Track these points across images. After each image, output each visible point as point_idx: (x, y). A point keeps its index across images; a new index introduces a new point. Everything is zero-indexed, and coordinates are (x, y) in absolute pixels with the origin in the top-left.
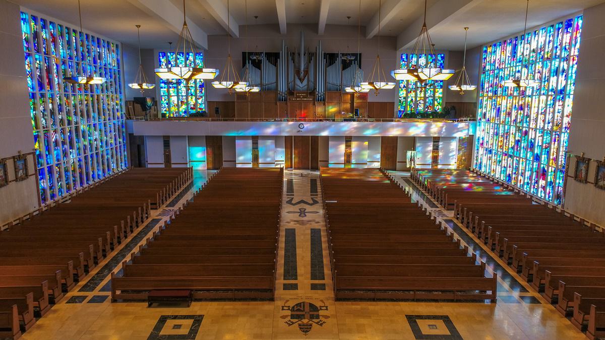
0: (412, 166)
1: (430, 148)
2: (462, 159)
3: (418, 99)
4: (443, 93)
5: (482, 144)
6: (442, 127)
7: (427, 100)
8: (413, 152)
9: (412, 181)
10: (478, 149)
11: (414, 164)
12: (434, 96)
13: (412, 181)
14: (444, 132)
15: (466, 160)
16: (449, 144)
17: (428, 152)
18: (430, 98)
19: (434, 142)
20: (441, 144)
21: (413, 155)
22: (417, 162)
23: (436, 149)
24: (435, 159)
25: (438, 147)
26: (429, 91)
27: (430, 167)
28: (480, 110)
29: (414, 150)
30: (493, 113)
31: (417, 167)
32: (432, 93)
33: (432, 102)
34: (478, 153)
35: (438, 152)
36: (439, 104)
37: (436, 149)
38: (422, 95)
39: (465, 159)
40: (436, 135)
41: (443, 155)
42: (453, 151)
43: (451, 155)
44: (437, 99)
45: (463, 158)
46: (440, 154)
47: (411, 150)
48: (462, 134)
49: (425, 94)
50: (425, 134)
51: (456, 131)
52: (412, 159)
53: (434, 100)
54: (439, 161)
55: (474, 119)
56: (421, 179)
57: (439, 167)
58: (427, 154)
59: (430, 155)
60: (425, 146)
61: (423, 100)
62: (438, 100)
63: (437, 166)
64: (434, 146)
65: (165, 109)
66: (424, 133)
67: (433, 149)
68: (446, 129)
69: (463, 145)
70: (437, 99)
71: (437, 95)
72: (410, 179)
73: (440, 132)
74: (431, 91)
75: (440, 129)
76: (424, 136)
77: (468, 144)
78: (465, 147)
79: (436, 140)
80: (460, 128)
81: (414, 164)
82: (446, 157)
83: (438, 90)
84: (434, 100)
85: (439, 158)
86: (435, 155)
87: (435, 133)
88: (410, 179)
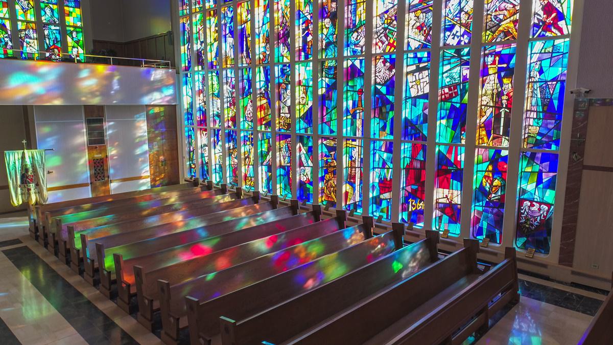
0: (34, 198)
1: (82, 139)
2: (158, 161)
3: (21, 26)
4: (83, 18)
5: (203, 122)
6: (109, 78)
7: (46, 32)
8: (28, 153)
9: (40, 251)
10: (190, 136)
11: (40, 192)
12: (62, 23)
13: (40, 251)
14: (116, 91)
15: (169, 162)
16: (132, 127)
17: (78, 149)
18: (53, 27)
19: (89, 122)
20: (110, 127)
21: (28, 161)
22: (48, 183)
23: (97, 140)
24: (99, 168)
25: (102, 134)
26: (48, 11)
27: (88, 193)
28: (183, 49)
29: (31, 145)
30: (228, 46)
31: (51, 198)
32: (56, 15)
33: (58, 36)
34: (190, 144)
35: (104, 150)
36: (77, 42)
37: (97, 140)
38: (31, 17)
39: (165, 160)
40: (96, 101)
41: (120, 156)
42: (140, 144)
43: (138, 151)
44: (71, 33)
45: (162, 158)
46: (112, 152)
47: (21, 147)
48: (157, 98)
49: (38, 15)
50: (62, 96)
51: (145, 89)
52: (28, 177)
53: (64, 32)
54: (111, 171)
55: (170, 62)
56: (78, 245)
57: (114, 186)
58: (76, 155)
59: (84, 159)
60: (65, 134)
61: (35, 31)
62: (74, 34)
63: (106, 183)
64: (90, 132)
65: (454, 194)
66: (57, 92)
67: (90, 142)
68: (120, 81)
69: (156, 129)
70: (71, 33)
71: (69, 20)
72: (31, 245)
73: (105, 90)
74: (52, 10)
75: (105, 82)
76: (57, 102)
77: (168, 122)
78: (162, 133)
79: (94, 116)
80: (154, 82)
81: (40, 192)
82: (128, 158)
83: (71, 9)
84: (64, 32)
85: (110, 163)
86: (98, 156)
87: (93, 94)
88: (31, 245)
